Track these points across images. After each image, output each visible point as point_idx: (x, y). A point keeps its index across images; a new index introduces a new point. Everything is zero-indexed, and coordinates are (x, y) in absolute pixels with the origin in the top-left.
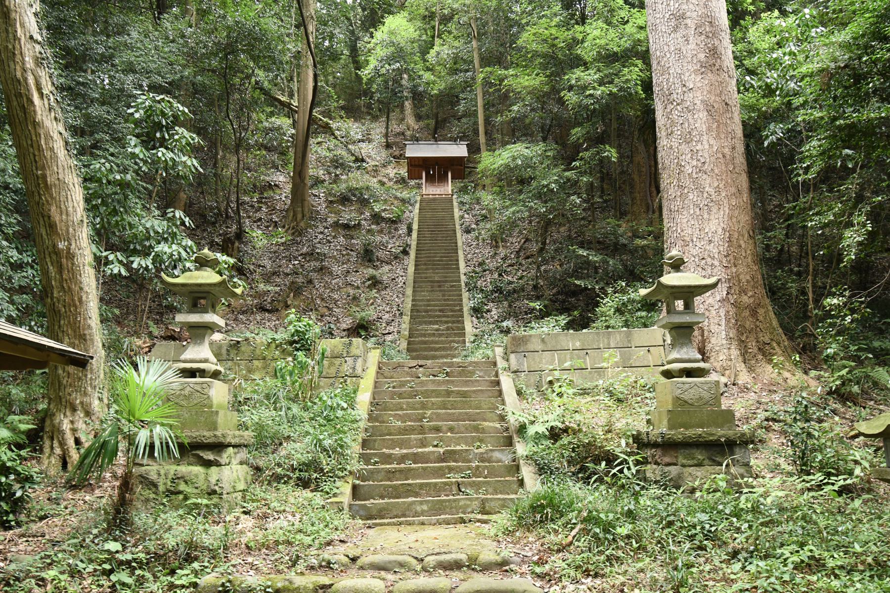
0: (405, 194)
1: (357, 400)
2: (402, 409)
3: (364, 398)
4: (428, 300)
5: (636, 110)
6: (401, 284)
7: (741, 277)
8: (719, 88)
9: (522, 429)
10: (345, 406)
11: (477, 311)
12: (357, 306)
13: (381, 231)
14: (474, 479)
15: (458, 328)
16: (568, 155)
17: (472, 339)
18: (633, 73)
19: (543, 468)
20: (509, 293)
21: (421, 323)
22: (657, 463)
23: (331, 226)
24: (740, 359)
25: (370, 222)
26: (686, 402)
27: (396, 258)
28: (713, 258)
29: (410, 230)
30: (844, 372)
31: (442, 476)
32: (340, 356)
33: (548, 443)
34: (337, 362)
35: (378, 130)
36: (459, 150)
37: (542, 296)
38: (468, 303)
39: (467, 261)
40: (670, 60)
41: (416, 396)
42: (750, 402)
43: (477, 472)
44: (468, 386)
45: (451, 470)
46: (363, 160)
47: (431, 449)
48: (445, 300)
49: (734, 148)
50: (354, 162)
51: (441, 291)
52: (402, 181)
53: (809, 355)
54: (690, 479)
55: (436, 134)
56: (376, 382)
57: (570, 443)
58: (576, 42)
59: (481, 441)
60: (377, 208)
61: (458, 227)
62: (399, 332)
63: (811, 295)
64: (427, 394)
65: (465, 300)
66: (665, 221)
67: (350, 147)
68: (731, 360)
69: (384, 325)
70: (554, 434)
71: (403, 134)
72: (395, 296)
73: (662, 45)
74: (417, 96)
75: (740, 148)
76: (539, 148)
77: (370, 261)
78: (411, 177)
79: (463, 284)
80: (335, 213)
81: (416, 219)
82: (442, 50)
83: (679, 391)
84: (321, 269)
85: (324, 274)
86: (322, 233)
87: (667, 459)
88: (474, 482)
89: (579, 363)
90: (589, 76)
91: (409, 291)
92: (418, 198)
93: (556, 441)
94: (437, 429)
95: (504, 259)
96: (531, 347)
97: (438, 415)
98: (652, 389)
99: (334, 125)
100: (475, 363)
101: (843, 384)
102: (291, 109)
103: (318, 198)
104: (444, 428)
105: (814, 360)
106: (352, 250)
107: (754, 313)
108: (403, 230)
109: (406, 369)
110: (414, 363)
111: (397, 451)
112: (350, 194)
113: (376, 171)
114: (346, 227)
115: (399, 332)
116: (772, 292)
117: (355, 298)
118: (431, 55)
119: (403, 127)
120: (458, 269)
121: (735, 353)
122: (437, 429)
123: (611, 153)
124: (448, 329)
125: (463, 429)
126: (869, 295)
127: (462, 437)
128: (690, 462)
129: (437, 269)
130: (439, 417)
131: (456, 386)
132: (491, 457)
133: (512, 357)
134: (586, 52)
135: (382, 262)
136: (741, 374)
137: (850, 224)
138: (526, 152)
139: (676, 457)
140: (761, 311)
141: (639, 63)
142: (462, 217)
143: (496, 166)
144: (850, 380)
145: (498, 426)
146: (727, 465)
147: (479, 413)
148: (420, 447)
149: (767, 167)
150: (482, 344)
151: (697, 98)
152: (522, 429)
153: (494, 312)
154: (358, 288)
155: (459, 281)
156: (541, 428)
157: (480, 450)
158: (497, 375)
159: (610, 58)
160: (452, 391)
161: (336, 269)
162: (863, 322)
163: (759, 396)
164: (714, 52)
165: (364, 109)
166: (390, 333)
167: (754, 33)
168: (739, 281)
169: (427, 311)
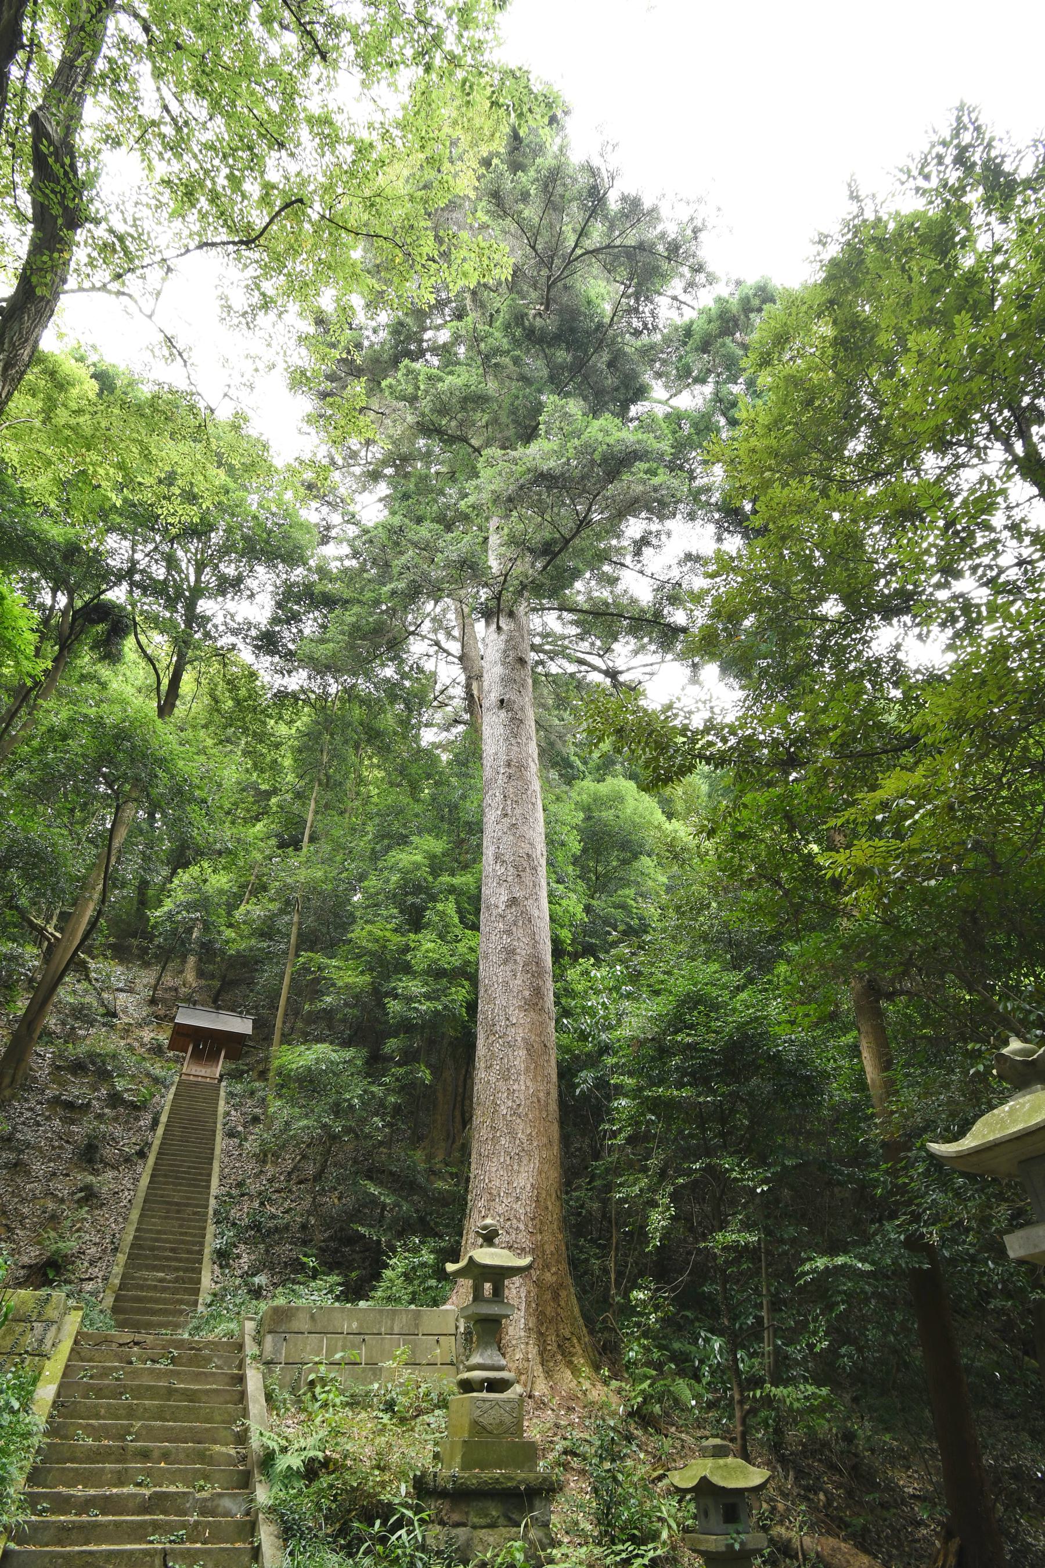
0: (157, 1071)
1: (36, 1396)
2: (98, 1417)
3: (46, 1392)
4: (159, 1232)
5: (456, 1030)
6: (125, 1202)
7: (546, 1247)
8: (538, 1028)
9: (268, 1459)
10: (16, 1405)
11: (223, 1256)
12: (55, 1229)
13: (116, 1119)
14: (188, 1545)
15: (191, 1281)
16: (375, 1064)
17: (209, 1299)
18: (460, 994)
19: (290, 1529)
20: (270, 1232)
21: (140, 1268)
22: (442, 1523)
23: (48, 1101)
24: (538, 1359)
25: (103, 1104)
26: (484, 1428)
27: (127, 1160)
28: (519, 1220)
29: (155, 1122)
30: (645, 1385)
31: (142, 1539)
32: (26, 1319)
33: (301, 1484)
34: (19, 1328)
35: (146, 978)
36: (242, 1025)
37: (311, 1241)
38: (212, 1243)
39: (222, 1177)
40: (497, 990)
41: (121, 1394)
42: (548, 1425)
43: (194, 1532)
44: (199, 1382)
45: (156, 1526)
46: (114, 1015)
47: (131, 1489)
48: (181, 1234)
49: (548, 1094)
50: (103, 1016)
51: (177, 1219)
52: (157, 1050)
53: (606, 1354)
54: (480, 1548)
55: (219, 1000)
56: (67, 1366)
57: (331, 1486)
58: (407, 949)
59: (206, 1477)
60: (120, 1085)
61: (219, 1126)
62: (105, 1279)
63: (613, 1276)
64: (138, 1392)
65: (209, 1237)
66: (473, 1166)
67: (105, 995)
68: (528, 1360)
69: (86, 1264)
70: (312, 1470)
71: (176, 990)
72: (112, 1220)
73: (493, 973)
74: (208, 951)
75: (554, 1094)
76: (348, 1054)
77: (91, 1161)
78: (171, 1047)
79: (211, 1212)
80: (59, 1084)
81: (167, 1108)
82: (252, 910)
83: (478, 1412)
84: (16, 1165)
85: (17, 1173)
86: (30, 1109)
87: (456, 1517)
88: (189, 1549)
89: (353, 1355)
90: (415, 987)
91: (135, 1215)
92: (177, 1079)
93: (311, 1481)
94: (145, 1455)
95: (270, 1181)
96: (295, 1325)
97: (150, 1429)
98: (443, 1404)
99: (92, 965)
100: (213, 1343)
101: (645, 1402)
102: (43, 935)
103: (42, 1057)
104: (156, 1454)
105: (614, 1364)
106: (68, 1142)
107: (556, 1297)
108: (146, 1121)
109: (114, 1346)
110: (127, 1337)
111: (79, 1491)
112: (87, 1060)
113: (127, 1031)
114: (70, 1106)
115: (105, 1279)
116: (574, 1263)
117: (54, 1218)
118: (239, 914)
119: (178, 982)
120: (208, 1187)
121: (533, 1351)
122: (145, 1455)
123: (425, 1074)
124: (176, 1280)
125: (182, 1456)
126: (673, 1290)
127: (180, 1470)
128: (483, 1521)
129: (180, 1184)
130: (150, 1434)
131: (182, 1382)
132: (218, 1506)
133: (269, 1338)
134: (417, 961)
135: (107, 1164)
136: (538, 1381)
137: (654, 1204)
138: (334, 1056)
139: (467, 1513)
140: (563, 1294)
141: (466, 983)
142: (228, 1114)
143: (294, 1066)
144: (652, 1397)
145: (233, 1452)
146: (526, 1526)
147: (207, 1430)
148: (115, 1486)
149: (578, 1115)
150: (224, 1310)
151: (518, 1034)
152: (268, 1459)
153: (245, 1258)
154: (62, 1201)
155: (207, 1207)
156: (294, 1461)
157: (204, 1494)
158: (241, 1366)
159: (437, 973)
160: (177, 1390)
161: (38, 1168)
162: (666, 1321)
163: (557, 1416)
164: (538, 992)
165: (135, 951)
166: (90, 1279)
167: (572, 974)
168: (543, 1252)
169: (152, 1249)
